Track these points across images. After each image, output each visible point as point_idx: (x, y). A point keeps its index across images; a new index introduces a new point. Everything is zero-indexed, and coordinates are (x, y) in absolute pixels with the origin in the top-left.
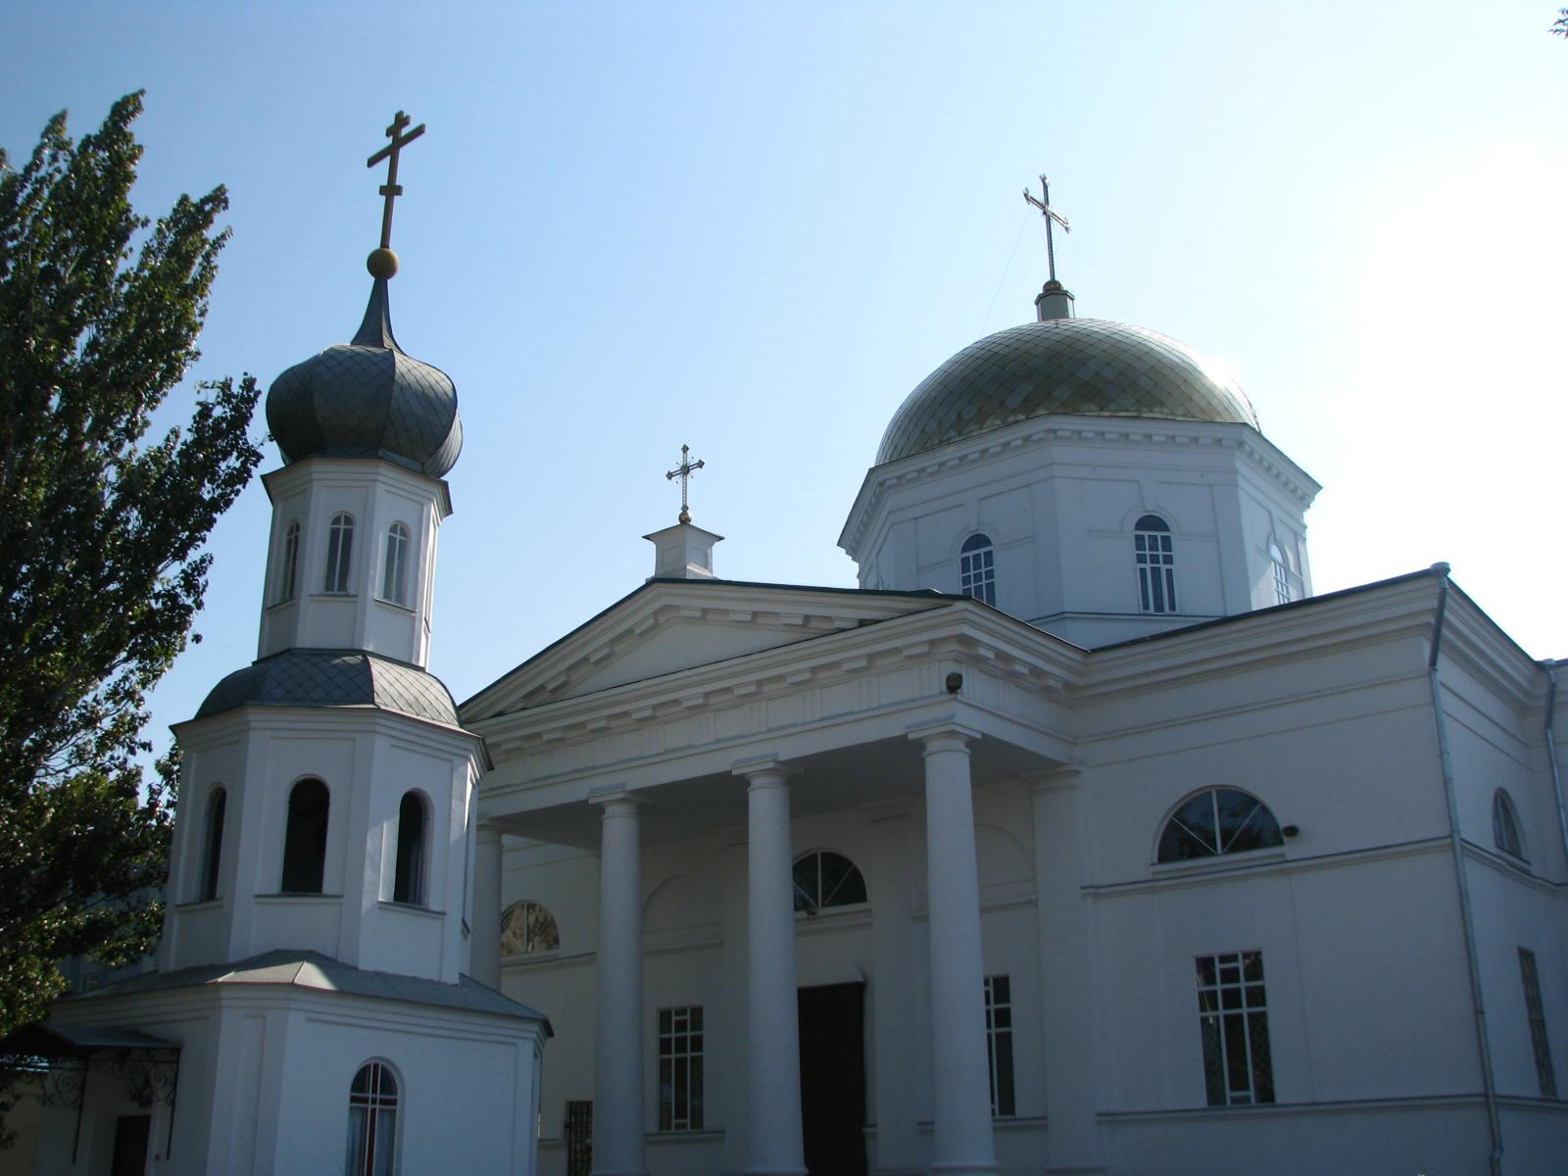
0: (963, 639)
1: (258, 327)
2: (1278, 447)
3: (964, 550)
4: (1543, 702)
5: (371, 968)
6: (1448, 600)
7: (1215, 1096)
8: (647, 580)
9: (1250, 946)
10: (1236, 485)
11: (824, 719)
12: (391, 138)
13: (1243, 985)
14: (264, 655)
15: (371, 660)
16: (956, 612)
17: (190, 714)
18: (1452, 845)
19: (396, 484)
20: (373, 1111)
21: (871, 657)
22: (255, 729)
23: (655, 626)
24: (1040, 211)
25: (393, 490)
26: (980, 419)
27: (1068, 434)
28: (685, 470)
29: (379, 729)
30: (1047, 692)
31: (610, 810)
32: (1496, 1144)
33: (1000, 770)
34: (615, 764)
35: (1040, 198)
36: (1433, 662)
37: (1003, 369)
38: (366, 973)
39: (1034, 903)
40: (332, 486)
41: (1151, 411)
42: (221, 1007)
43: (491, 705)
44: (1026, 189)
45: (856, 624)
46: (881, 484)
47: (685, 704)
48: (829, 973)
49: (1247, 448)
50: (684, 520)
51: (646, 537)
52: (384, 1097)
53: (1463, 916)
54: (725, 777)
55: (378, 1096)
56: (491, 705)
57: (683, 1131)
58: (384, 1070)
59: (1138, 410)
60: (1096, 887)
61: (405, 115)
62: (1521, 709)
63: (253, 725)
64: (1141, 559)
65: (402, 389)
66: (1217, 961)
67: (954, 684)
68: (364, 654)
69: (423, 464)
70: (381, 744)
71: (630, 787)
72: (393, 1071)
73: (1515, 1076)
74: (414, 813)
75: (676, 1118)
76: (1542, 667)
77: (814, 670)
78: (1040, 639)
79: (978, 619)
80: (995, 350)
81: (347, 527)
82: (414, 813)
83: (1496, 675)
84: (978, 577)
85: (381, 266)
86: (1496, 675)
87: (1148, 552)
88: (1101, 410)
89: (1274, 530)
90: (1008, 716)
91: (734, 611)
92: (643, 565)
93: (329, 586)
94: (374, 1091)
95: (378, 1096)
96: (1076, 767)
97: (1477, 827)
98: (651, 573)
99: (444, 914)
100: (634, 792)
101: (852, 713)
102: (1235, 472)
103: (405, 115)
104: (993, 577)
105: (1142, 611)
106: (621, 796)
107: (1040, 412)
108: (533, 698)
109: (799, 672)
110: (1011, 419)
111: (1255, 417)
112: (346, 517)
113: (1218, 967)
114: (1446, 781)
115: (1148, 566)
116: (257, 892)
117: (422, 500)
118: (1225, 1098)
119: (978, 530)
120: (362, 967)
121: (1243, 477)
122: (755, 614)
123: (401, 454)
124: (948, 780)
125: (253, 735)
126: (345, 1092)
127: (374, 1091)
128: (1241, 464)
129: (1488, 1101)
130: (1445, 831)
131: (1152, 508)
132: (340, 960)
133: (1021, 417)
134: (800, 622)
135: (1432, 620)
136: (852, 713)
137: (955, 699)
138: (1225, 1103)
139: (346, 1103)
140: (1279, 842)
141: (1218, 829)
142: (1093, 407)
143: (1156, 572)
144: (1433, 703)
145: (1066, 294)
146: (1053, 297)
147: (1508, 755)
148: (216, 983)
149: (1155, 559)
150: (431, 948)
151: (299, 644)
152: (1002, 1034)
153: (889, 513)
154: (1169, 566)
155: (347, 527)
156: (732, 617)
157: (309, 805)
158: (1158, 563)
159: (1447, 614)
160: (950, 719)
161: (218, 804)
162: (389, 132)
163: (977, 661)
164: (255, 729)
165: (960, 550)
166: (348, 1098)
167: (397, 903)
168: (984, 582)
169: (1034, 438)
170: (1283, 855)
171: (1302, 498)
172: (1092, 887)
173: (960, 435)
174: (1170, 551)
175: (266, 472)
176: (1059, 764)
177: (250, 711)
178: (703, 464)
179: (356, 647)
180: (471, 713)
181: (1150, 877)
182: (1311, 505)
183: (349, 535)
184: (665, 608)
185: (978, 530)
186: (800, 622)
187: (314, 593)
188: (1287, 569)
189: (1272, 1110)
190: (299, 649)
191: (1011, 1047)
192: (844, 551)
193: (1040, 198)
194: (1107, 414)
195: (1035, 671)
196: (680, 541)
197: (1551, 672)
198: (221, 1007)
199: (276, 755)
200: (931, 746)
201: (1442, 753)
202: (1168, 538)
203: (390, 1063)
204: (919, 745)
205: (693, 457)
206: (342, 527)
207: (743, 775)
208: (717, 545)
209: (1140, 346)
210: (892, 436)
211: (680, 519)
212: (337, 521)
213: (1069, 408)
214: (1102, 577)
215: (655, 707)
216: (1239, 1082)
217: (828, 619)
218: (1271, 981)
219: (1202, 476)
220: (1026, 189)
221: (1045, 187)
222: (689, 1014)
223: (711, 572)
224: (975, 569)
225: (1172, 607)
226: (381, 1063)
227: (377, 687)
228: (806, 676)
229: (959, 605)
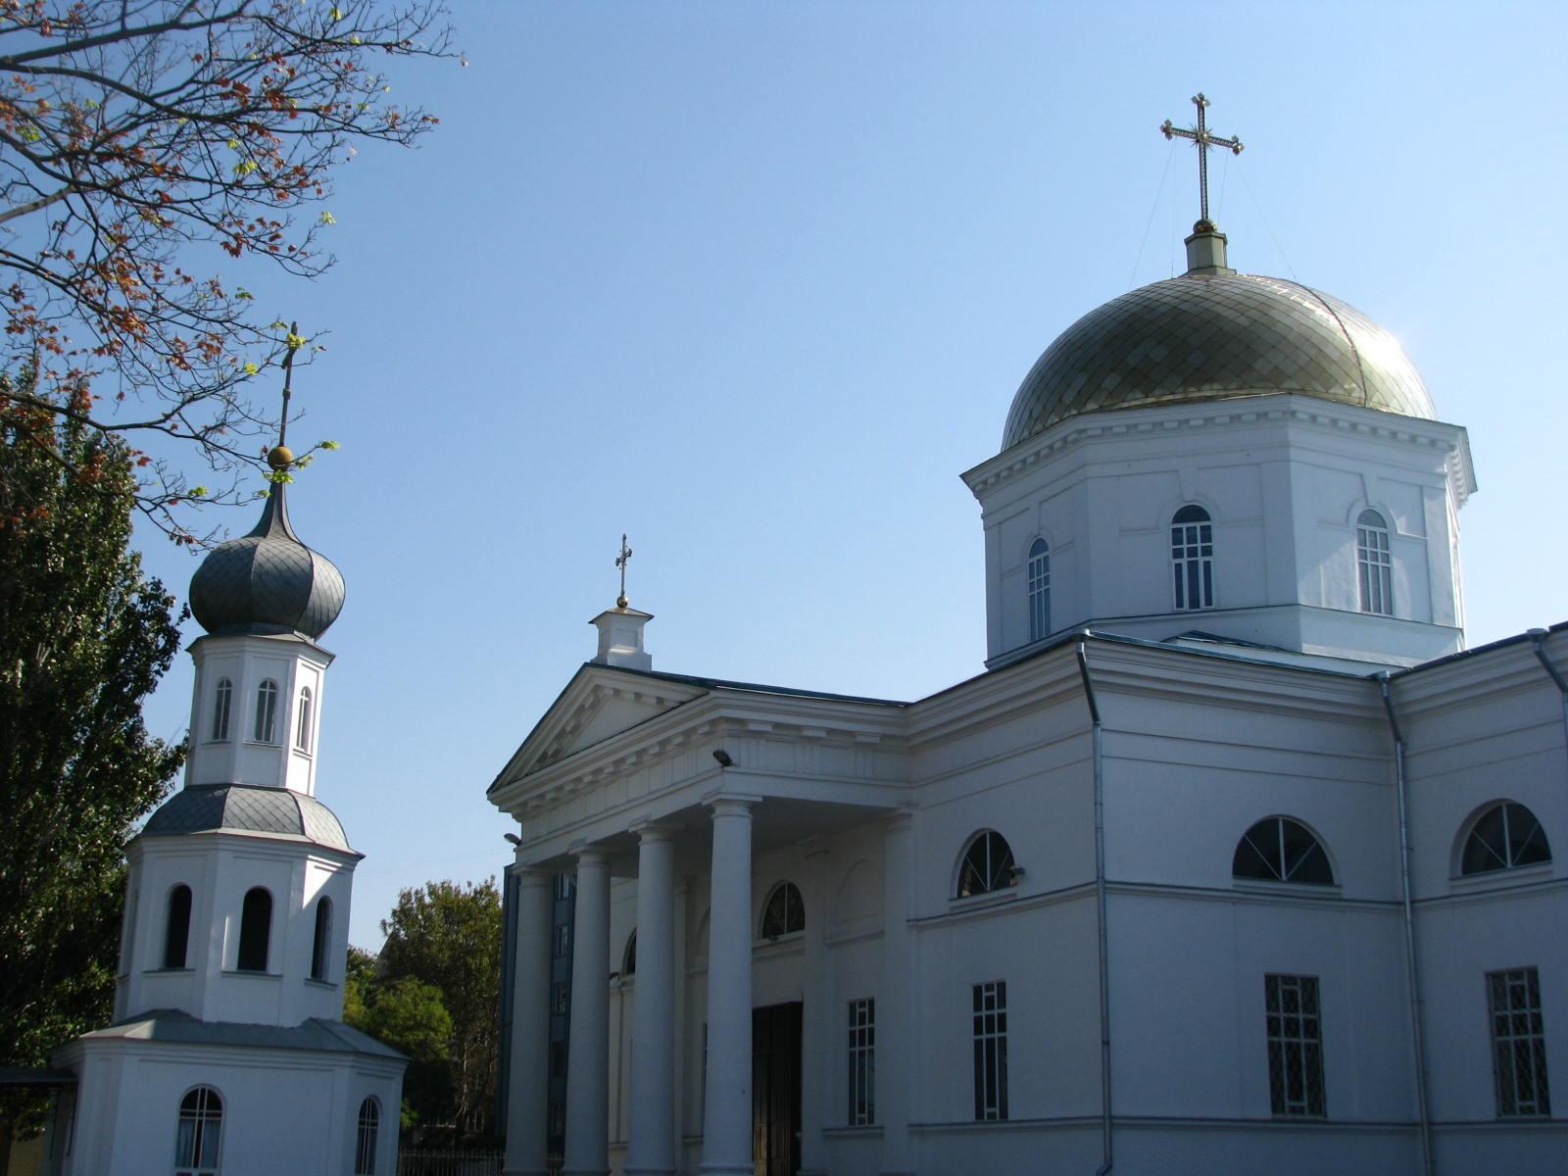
3: (1032, 555)
5: (214, 1019)
19: (266, 651)
20: (200, 1122)
34: (583, 820)
38: (208, 1024)
40: (252, 660)
41: (1199, 390)
43: (522, 769)
50: (622, 604)
51: (591, 622)
52: (210, 1111)
55: (198, 1111)
56: (522, 769)
59: (1185, 392)
63: (145, 849)
64: (1178, 554)
78: (1004, 664)
79: (735, 702)
88: (1147, 397)
90: (806, 776)
93: (216, 736)
94: (202, 1107)
95: (198, 1111)
99: (281, 976)
104: (1174, 550)
105: (1175, 609)
107: (1091, 406)
108: (544, 760)
115: (1184, 561)
116: (145, 969)
117: (287, 658)
118: (983, 1114)
119: (1039, 535)
127: (202, 1107)
131: (1190, 498)
143: (1193, 566)
154: (1207, 559)
157: (181, 901)
158: (1189, 556)
166: (179, 1114)
167: (241, 971)
170: (1014, 895)
175: (187, 647)
180: (512, 774)
185: (1039, 535)
187: (205, 742)
194: (1150, 400)
196: (620, 620)
200: (719, 810)
204: (710, 809)
206: (224, 689)
207: (635, 832)
208: (648, 626)
212: (263, 685)
219: (1248, 455)
225: (1209, 602)
226: (207, 1088)
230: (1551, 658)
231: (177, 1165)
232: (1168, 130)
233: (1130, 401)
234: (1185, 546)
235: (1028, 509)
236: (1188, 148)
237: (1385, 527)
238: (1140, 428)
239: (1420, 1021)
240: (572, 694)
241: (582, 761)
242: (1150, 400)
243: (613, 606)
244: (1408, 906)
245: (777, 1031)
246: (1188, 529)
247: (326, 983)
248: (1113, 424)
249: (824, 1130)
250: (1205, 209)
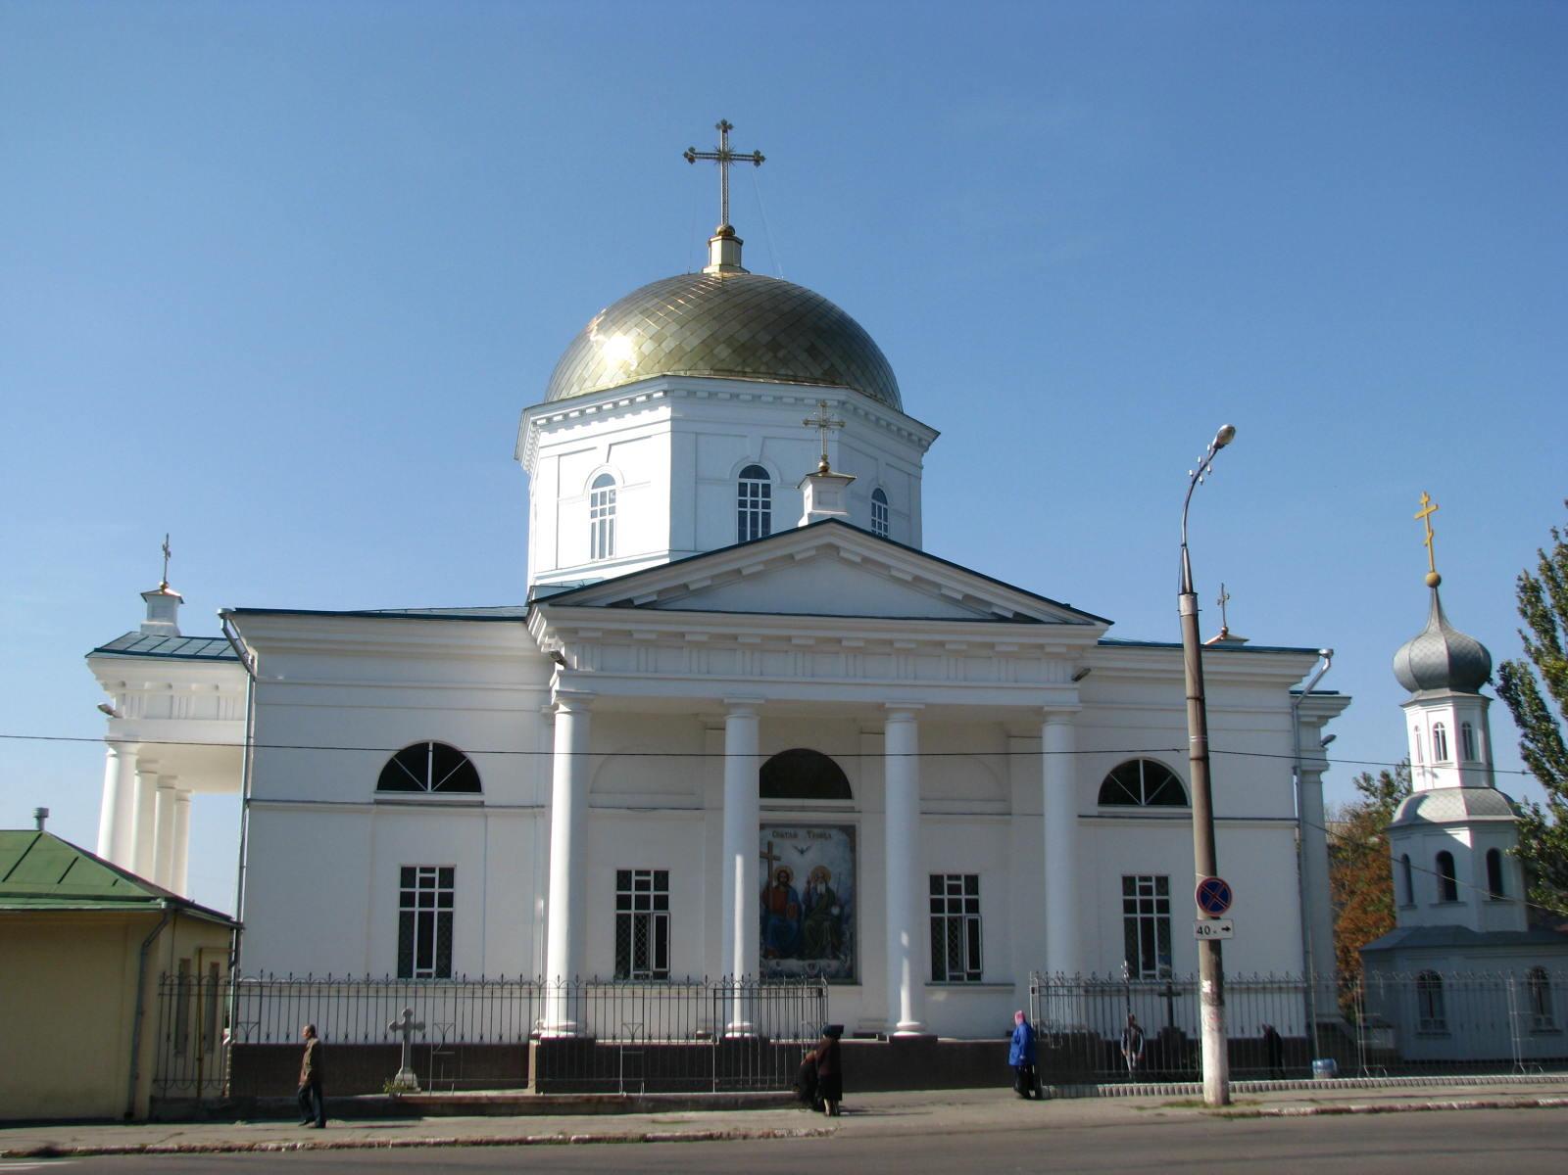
7: (404, 971)
13: (437, 890)
48: (642, 859)
64: (593, 515)
66: (945, 878)
75: (418, 967)
113: (418, 875)
115: (597, 520)
141: (1137, 785)
143: (602, 523)
152: (956, 912)
178: (724, 123)
191: (932, 924)
202: (769, 485)
216: (425, 961)
218: (984, 897)
224: (601, 504)
232: (758, 159)
234: (599, 508)
235: (595, 448)
237: (886, 503)
240: (631, 583)
246: (763, 485)
247: (1459, 903)
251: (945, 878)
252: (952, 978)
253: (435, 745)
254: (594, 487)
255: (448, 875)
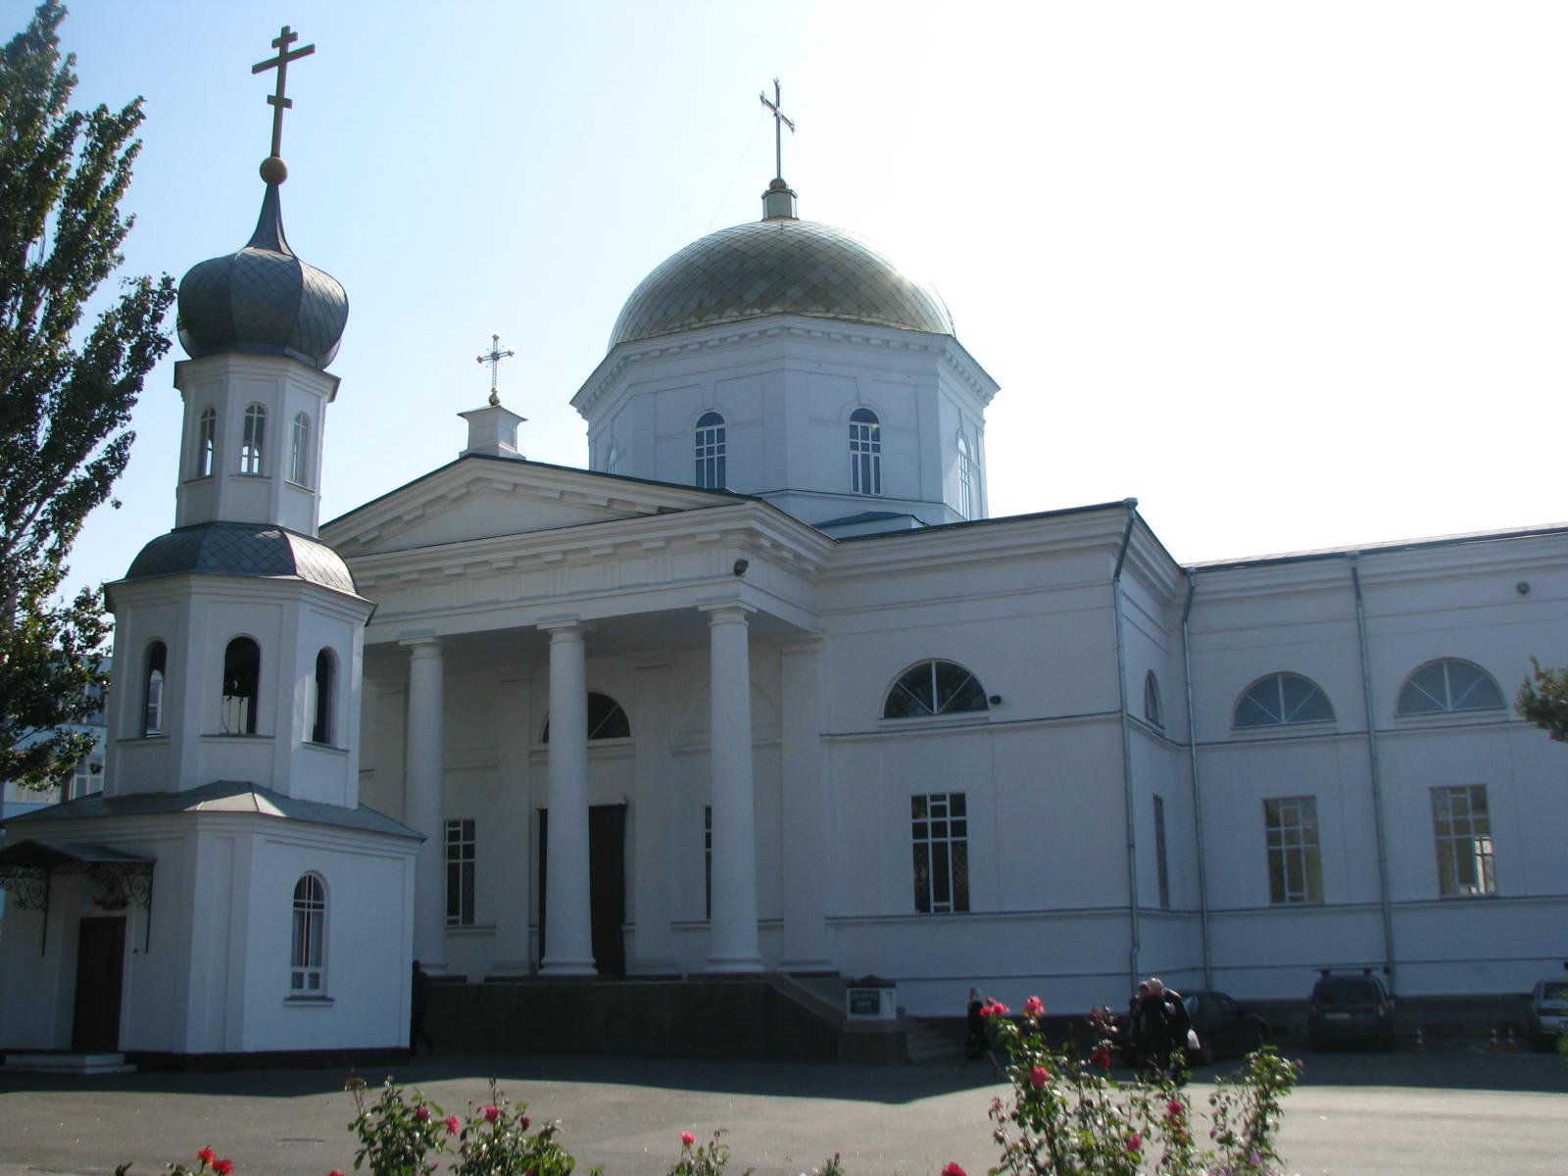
0: (750, 532)
1: (175, 222)
2: (972, 356)
4: (1183, 600)
5: (298, 797)
6: (1134, 528)
7: (922, 905)
8: (461, 453)
9: (957, 789)
10: (937, 387)
11: (621, 588)
12: (278, 49)
13: (949, 819)
14: (182, 525)
15: (290, 537)
16: (746, 510)
17: (119, 572)
18: (1122, 718)
21: (668, 540)
22: (195, 593)
23: (468, 493)
24: (772, 113)
25: (299, 385)
26: (720, 308)
27: (800, 332)
28: (495, 356)
29: (303, 597)
30: (802, 573)
31: (419, 652)
32: (1135, 943)
33: (770, 638)
35: (773, 101)
36: (1117, 574)
37: (742, 265)
38: (295, 800)
39: (779, 746)
40: (245, 379)
42: (197, 831)
44: (763, 92)
45: (654, 511)
46: (626, 358)
47: (495, 566)
48: (609, 797)
49: (948, 355)
50: (494, 401)
51: (460, 415)
52: (315, 902)
53: (1125, 773)
54: (531, 630)
55: (312, 902)
57: (454, 926)
58: (316, 881)
59: (859, 315)
60: (832, 735)
61: (291, 32)
62: (1164, 602)
63: (194, 590)
64: (854, 446)
65: (308, 296)
66: (929, 798)
67: (740, 568)
68: (281, 530)
69: (317, 360)
70: (304, 610)
71: (439, 633)
72: (323, 885)
73: (1148, 898)
74: (325, 665)
76: (1184, 572)
77: (616, 546)
78: (787, 521)
80: (734, 246)
81: (260, 416)
82: (325, 665)
83: (1156, 582)
84: (710, 451)
85: (273, 173)
86: (1156, 582)
87: (860, 441)
88: (828, 311)
89: (962, 427)
91: (543, 489)
92: (454, 442)
96: (820, 636)
97: (1136, 707)
98: (464, 446)
99: (347, 751)
100: (439, 637)
101: (647, 585)
102: (936, 375)
103: (291, 32)
104: (724, 452)
106: (431, 640)
107: (775, 309)
109: (602, 547)
110: (748, 312)
111: (952, 324)
112: (259, 407)
114: (1121, 669)
115: (859, 453)
116: (202, 733)
120: (292, 795)
121: (943, 380)
122: (562, 493)
123: (301, 351)
124: (730, 645)
125: (194, 598)
126: (290, 899)
127: (309, 898)
128: (943, 371)
129: (1132, 912)
130: (1118, 708)
131: (866, 402)
132: (274, 790)
133: (757, 311)
134: (605, 503)
135: (1121, 542)
136: (647, 585)
137: (740, 581)
138: (929, 910)
139: (291, 908)
140: (984, 707)
141: (938, 690)
142: (821, 309)
143: (866, 458)
144: (1115, 607)
145: (790, 193)
146: (778, 195)
147: (1149, 637)
148: (195, 812)
149: (865, 447)
150: (331, 779)
151: (220, 518)
153: (631, 385)
154: (877, 455)
155: (260, 416)
156: (542, 493)
158: (868, 450)
159: (1132, 539)
160: (737, 595)
161: (157, 656)
162: (275, 44)
163: (756, 548)
164: (195, 593)
165: (695, 425)
168: (716, 456)
169: (770, 333)
170: (987, 718)
171: (984, 397)
172: (828, 735)
173: (700, 321)
174: (879, 440)
176: (808, 632)
177: (192, 577)
179: (272, 522)
181: (877, 729)
182: (990, 403)
183: (261, 422)
184: (478, 480)
186: (605, 503)
188: (969, 460)
189: (968, 917)
190: (221, 522)
192: (576, 409)
193: (773, 101)
194: (831, 315)
195: (798, 557)
197: (1192, 578)
198: (197, 831)
199: (212, 616)
200: (717, 618)
201: (1119, 646)
203: (320, 875)
205: (502, 348)
206: (255, 415)
207: (545, 631)
208: (522, 424)
209: (863, 256)
210: (634, 312)
211: (490, 401)
212: (251, 410)
213: (797, 308)
214: (823, 463)
215: (466, 566)
216: (942, 895)
217: (631, 503)
220: (763, 92)
221: (778, 91)
222: (462, 825)
223: (516, 448)
225: (878, 490)
226: (313, 875)
227: (297, 561)
228: (609, 550)
229: (750, 504)
230: (1361, 572)
231: (293, 965)
233: (813, 312)
234: (705, 446)
236: (488, 363)
238: (770, 333)
239: (1198, 834)
240: (425, 485)
241: (472, 550)
242: (831, 315)
243: (486, 404)
244: (1193, 743)
245: (608, 826)
248: (749, 331)
249: (673, 923)
250: (494, 382)
251: (929, 798)
252: (937, 909)
253: (938, 664)
254: (698, 426)
255: (959, 803)
